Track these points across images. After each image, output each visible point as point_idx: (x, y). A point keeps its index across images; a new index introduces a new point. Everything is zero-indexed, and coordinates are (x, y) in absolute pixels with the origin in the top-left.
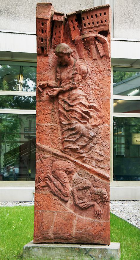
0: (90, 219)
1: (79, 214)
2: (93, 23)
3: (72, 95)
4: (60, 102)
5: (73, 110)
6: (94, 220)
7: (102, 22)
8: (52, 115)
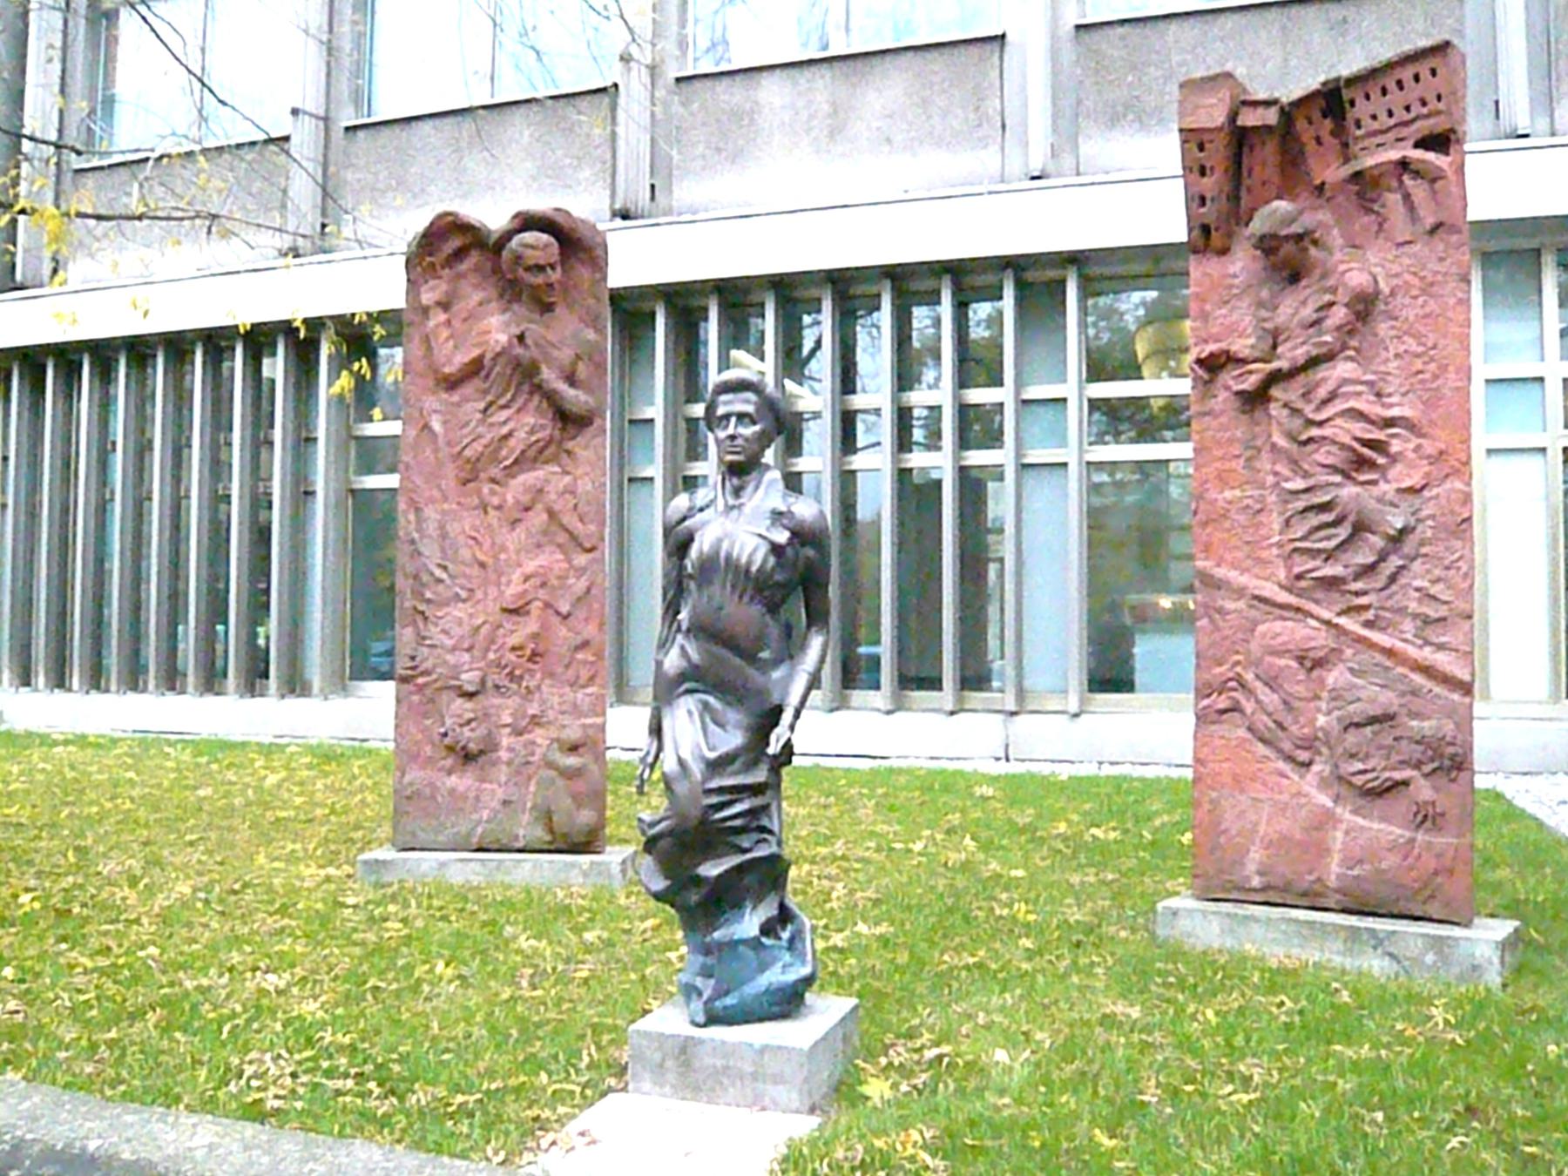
0: (1399, 831)
1: (1355, 812)
2: (1390, 114)
3: (1318, 385)
5: (1324, 438)
6: (1408, 834)
7: (1424, 103)
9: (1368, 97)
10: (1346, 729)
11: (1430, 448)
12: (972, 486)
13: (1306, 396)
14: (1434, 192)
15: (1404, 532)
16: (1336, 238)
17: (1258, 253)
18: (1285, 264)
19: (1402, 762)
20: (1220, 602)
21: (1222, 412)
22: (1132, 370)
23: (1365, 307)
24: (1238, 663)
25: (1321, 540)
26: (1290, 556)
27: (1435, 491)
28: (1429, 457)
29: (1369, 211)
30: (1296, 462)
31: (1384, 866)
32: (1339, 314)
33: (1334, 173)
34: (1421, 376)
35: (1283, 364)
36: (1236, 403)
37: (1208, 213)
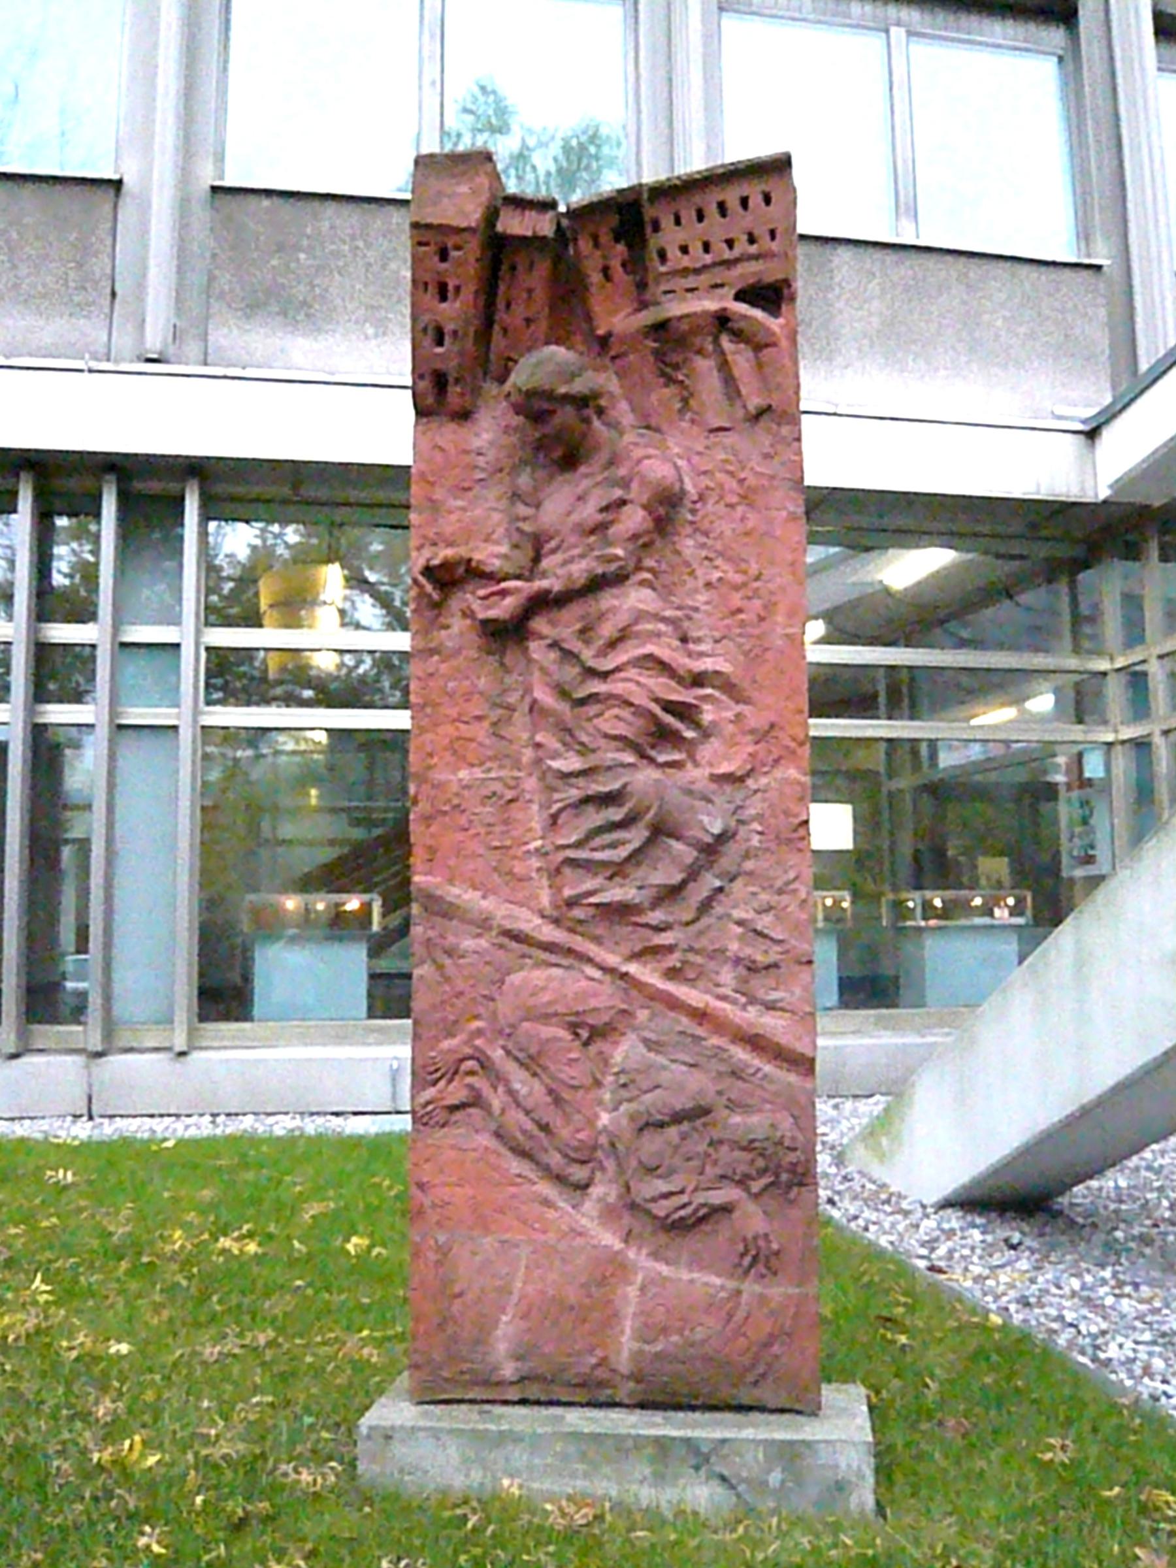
0: (718, 1281)
1: (655, 1255)
2: (707, 247)
3: (602, 616)
4: (535, 656)
5: (611, 696)
6: (731, 1284)
8: (494, 724)
9: (678, 222)
10: (641, 1130)
11: (756, 718)
12: (47, 751)
13: (585, 633)
14: (760, 366)
15: (723, 837)
16: (623, 412)
17: (518, 420)
18: (558, 437)
19: (723, 1177)
20: (451, 939)
21: (458, 651)
22: (253, 620)
23: (666, 509)
24: (479, 1032)
25: (603, 848)
26: (558, 871)
27: (764, 781)
28: (752, 732)
29: (670, 380)
30: (569, 731)
31: (700, 1334)
32: (634, 519)
33: (619, 318)
34: (742, 616)
35: (551, 583)
36: (474, 639)
37: (447, 355)
